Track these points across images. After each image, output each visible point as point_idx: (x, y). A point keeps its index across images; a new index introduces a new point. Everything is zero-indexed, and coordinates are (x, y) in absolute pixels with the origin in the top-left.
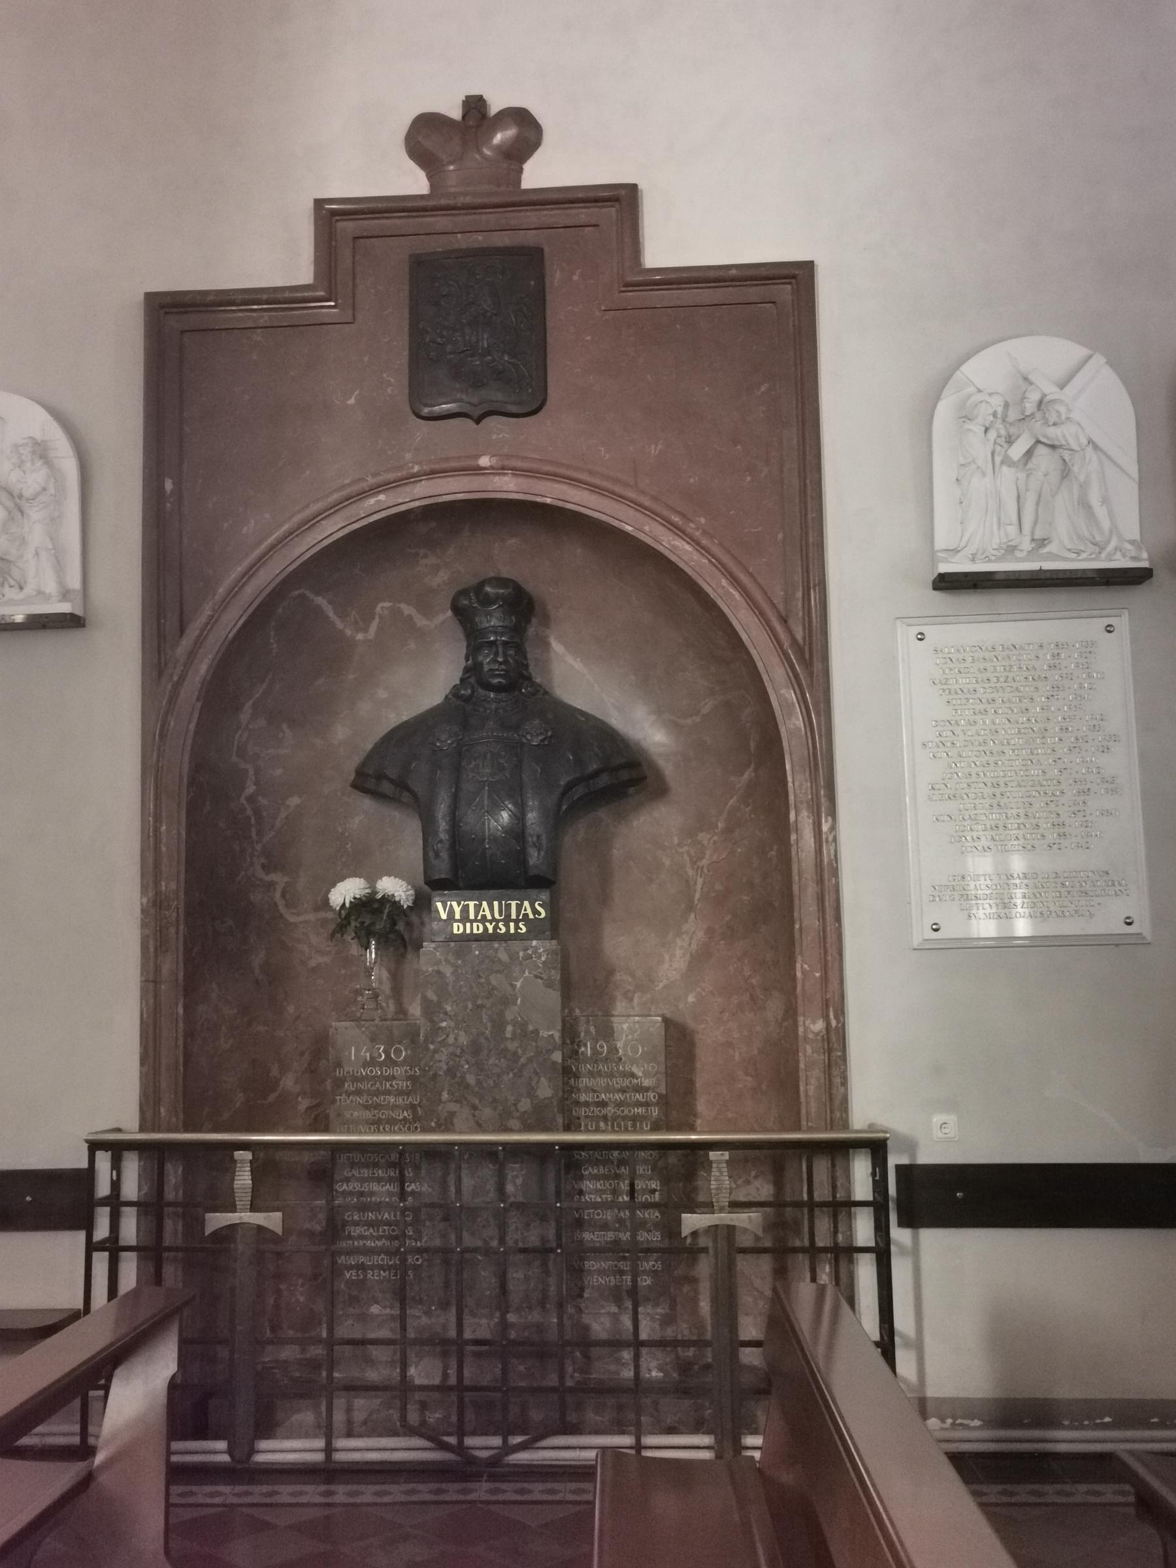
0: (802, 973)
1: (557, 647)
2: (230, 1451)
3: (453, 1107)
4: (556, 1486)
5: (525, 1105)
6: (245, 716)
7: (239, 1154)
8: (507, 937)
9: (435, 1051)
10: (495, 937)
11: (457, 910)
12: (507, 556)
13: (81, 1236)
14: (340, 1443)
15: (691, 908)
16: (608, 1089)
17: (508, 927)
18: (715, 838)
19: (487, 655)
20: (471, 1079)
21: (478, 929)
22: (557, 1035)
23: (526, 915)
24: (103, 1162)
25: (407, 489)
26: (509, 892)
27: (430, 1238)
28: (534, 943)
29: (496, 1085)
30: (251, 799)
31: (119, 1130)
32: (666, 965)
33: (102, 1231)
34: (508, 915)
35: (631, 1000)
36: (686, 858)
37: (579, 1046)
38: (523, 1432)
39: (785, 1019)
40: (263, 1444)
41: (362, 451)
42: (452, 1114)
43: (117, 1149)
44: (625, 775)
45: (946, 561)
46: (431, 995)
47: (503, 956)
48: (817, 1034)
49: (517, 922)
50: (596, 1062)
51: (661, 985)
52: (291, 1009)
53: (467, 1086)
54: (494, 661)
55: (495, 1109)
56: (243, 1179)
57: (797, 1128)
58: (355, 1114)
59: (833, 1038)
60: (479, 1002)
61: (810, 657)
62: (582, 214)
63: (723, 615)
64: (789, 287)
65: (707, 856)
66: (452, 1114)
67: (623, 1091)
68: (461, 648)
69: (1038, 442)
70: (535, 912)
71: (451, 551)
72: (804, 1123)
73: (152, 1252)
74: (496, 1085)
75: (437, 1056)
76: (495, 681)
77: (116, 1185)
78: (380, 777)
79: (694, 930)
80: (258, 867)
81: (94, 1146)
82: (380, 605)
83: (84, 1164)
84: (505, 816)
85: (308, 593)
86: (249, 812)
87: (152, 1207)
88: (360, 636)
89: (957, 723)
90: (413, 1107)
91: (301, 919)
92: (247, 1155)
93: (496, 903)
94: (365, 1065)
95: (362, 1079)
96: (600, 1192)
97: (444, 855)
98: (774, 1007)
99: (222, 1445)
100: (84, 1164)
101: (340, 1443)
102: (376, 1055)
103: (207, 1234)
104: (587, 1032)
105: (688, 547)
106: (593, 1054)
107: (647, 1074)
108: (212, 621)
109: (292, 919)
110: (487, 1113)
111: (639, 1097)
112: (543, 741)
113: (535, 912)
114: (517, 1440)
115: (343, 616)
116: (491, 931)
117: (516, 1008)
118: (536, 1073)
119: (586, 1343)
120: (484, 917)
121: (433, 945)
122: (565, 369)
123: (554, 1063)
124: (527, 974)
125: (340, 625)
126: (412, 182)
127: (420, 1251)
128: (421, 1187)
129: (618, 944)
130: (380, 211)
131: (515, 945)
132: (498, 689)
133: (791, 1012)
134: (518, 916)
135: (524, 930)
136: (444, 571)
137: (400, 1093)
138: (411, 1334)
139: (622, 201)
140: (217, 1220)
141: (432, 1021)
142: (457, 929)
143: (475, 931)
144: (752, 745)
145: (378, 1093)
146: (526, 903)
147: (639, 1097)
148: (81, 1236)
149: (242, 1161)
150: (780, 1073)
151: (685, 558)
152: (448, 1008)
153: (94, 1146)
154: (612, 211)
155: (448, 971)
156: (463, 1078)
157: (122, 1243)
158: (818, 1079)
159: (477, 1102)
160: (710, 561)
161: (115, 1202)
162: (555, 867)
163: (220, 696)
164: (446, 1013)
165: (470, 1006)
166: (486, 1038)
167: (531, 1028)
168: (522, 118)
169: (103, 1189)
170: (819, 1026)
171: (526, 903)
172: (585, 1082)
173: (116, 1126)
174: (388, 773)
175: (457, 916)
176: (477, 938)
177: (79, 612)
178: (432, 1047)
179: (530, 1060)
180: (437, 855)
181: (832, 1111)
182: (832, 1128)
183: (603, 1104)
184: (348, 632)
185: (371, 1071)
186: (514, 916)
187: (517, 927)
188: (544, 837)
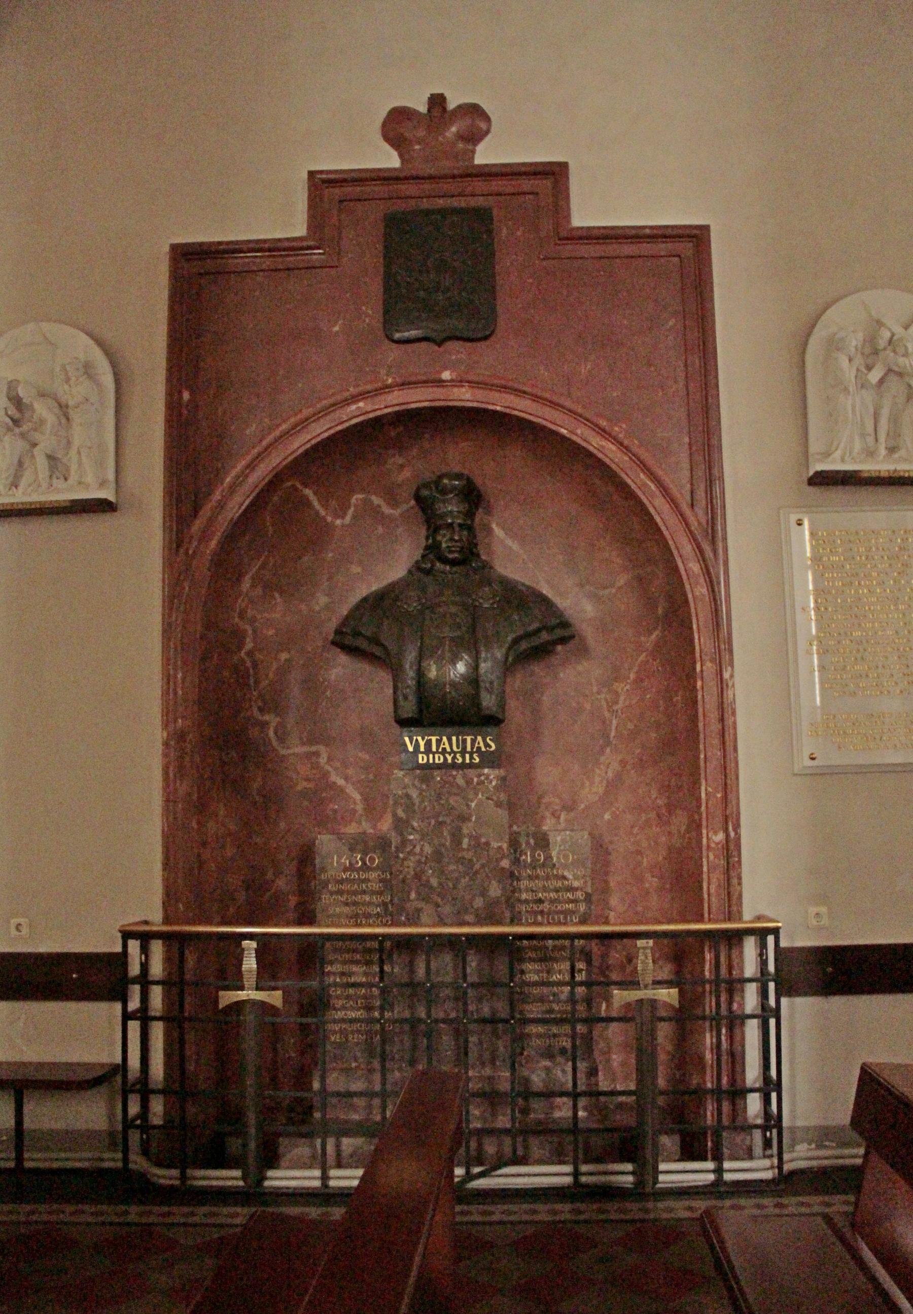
0: (706, 794)
1: (498, 532)
2: (244, 1178)
3: (421, 904)
4: (512, 1207)
5: (479, 902)
6: (246, 584)
7: (246, 943)
8: (463, 766)
9: (404, 859)
10: (454, 766)
11: (422, 744)
12: (457, 456)
13: (118, 1007)
14: (333, 1173)
15: (608, 743)
16: (545, 889)
17: (464, 758)
18: (628, 687)
19: (444, 536)
20: (434, 882)
21: (439, 759)
22: (505, 846)
23: (479, 748)
24: (134, 946)
25: (382, 397)
26: (466, 729)
27: (400, 1011)
28: (486, 771)
29: (455, 887)
30: (250, 653)
31: (146, 923)
32: (587, 790)
33: (134, 1004)
34: (465, 748)
35: (559, 818)
36: (603, 703)
37: (521, 855)
38: (481, 1164)
39: (688, 831)
40: (270, 1173)
41: (340, 371)
42: (419, 910)
43: (145, 938)
44: (559, 633)
45: (819, 461)
46: (401, 813)
47: (460, 781)
48: (717, 844)
49: (471, 754)
50: (534, 868)
51: (583, 806)
52: (282, 825)
53: (431, 887)
54: (452, 539)
55: (454, 905)
56: (250, 963)
57: (701, 920)
58: (338, 910)
59: (732, 847)
60: (441, 819)
61: (710, 535)
62: (526, 184)
63: (642, 504)
64: (691, 244)
65: (621, 702)
66: (419, 910)
67: (557, 891)
68: (423, 532)
69: (890, 370)
70: (487, 745)
71: (414, 452)
72: (706, 915)
73: (174, 1020)
74: (455, 887)
75: (406, 863)
76: (451, 556)
77: (145, 967)
78: (357, 634)
79: (610, 763)
80: (255, 711)
81: (127, 935)
82: (355, 497)
83: (119, 949)
84: (461, 667)
85: (299, 486)
86: (249, 664)
87: (174, 983)
88: (338, 522)
89: (829, 592)
90: (385, 904)
91: (291, 751)
92: (254, 944)
93: (454, 738)
94: (345, 870)
95: (341, 882)
96: (537, 972)
97: (412, 698)
98: (680, 821)
99: (237, 1173)
100: (119, 949)
101: (333, 1173)
102: (354, 862)
103: (221, 1007)
104: (528, 843)
105: (614, 448)
106: (532, 861)
107: (576, 878)
108: (221, 505)
109: (283, 752)
110: (447, 909)
111: (570, 895)
112: (492, 604)
113: (487, 745)
114: (477, 1170)
115: (326, 506)
116: (450, 761)
117: (470, 825)
118: (487, 876)
119: (528, 1094)
120: (444, 749)
121: (402, 773)
122: (509, 306)
123: (503, 869)
124: (480, 796)
125: (323, 512)
126: (391, 160)
127: (395, 1021)
128: (396, 969)
129: (547, 773)
130: (361, 180)
131: (471, 772)
132: (453, 563)
133: (696, 826)
134: (472, 748)
135: (477, 760)
136: (406, 469)
137: (373, 893)
138: (389, 1087)
139: (555, 174)
140: (228, 997)
141: (401, 834)
142: (422, 759)
143: (437, 761)
144: (660, 611)
145: (355, 893)
146: (479, 738)
147: (570, 895)
148: (118, 1007)
149: (249, 949)
150: (683, 879)
151: (611, 456)
152: (415, 824)
153: (127, 935)
154: (548, 183)
155: (414, 794)
156: (428, 881)
157: (152, 1013)
158: (718, 879)
159: (439, 900)
160: (631, 459)
161: (144, 980)
162: (502, 705)
163: (226, 567)
164: (413, 829)
165: (433, 822)
166: (447, 849)
167: (483, 840)
168: (474, 111)
169: (134, 969)
170: (720, 837)
171: (479, 738)
172: (524, 884)
173: (143, 918)
174: (364, 635)
175: (422, 749)
176: (439, 767)
177: (112, 498)
178: (401, 855)
179: (483, 866)
180: (406, 698)
181: (729, 906)
182: (729, 920)
183: (540, 901)
184: (329, 519)
185: (350, 875)
186: (469, 749)
187: (471, 758)
188: (495, 684)
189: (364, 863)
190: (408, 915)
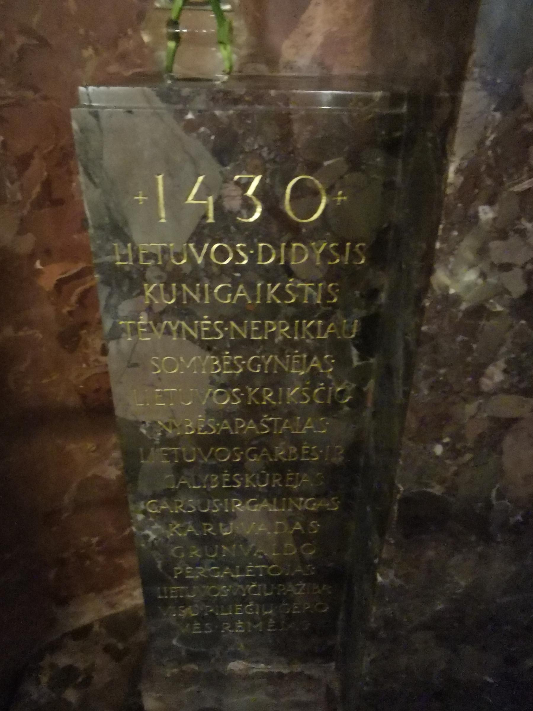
102: (233, 204)
189: (273, 209)
190: (458, 437)
